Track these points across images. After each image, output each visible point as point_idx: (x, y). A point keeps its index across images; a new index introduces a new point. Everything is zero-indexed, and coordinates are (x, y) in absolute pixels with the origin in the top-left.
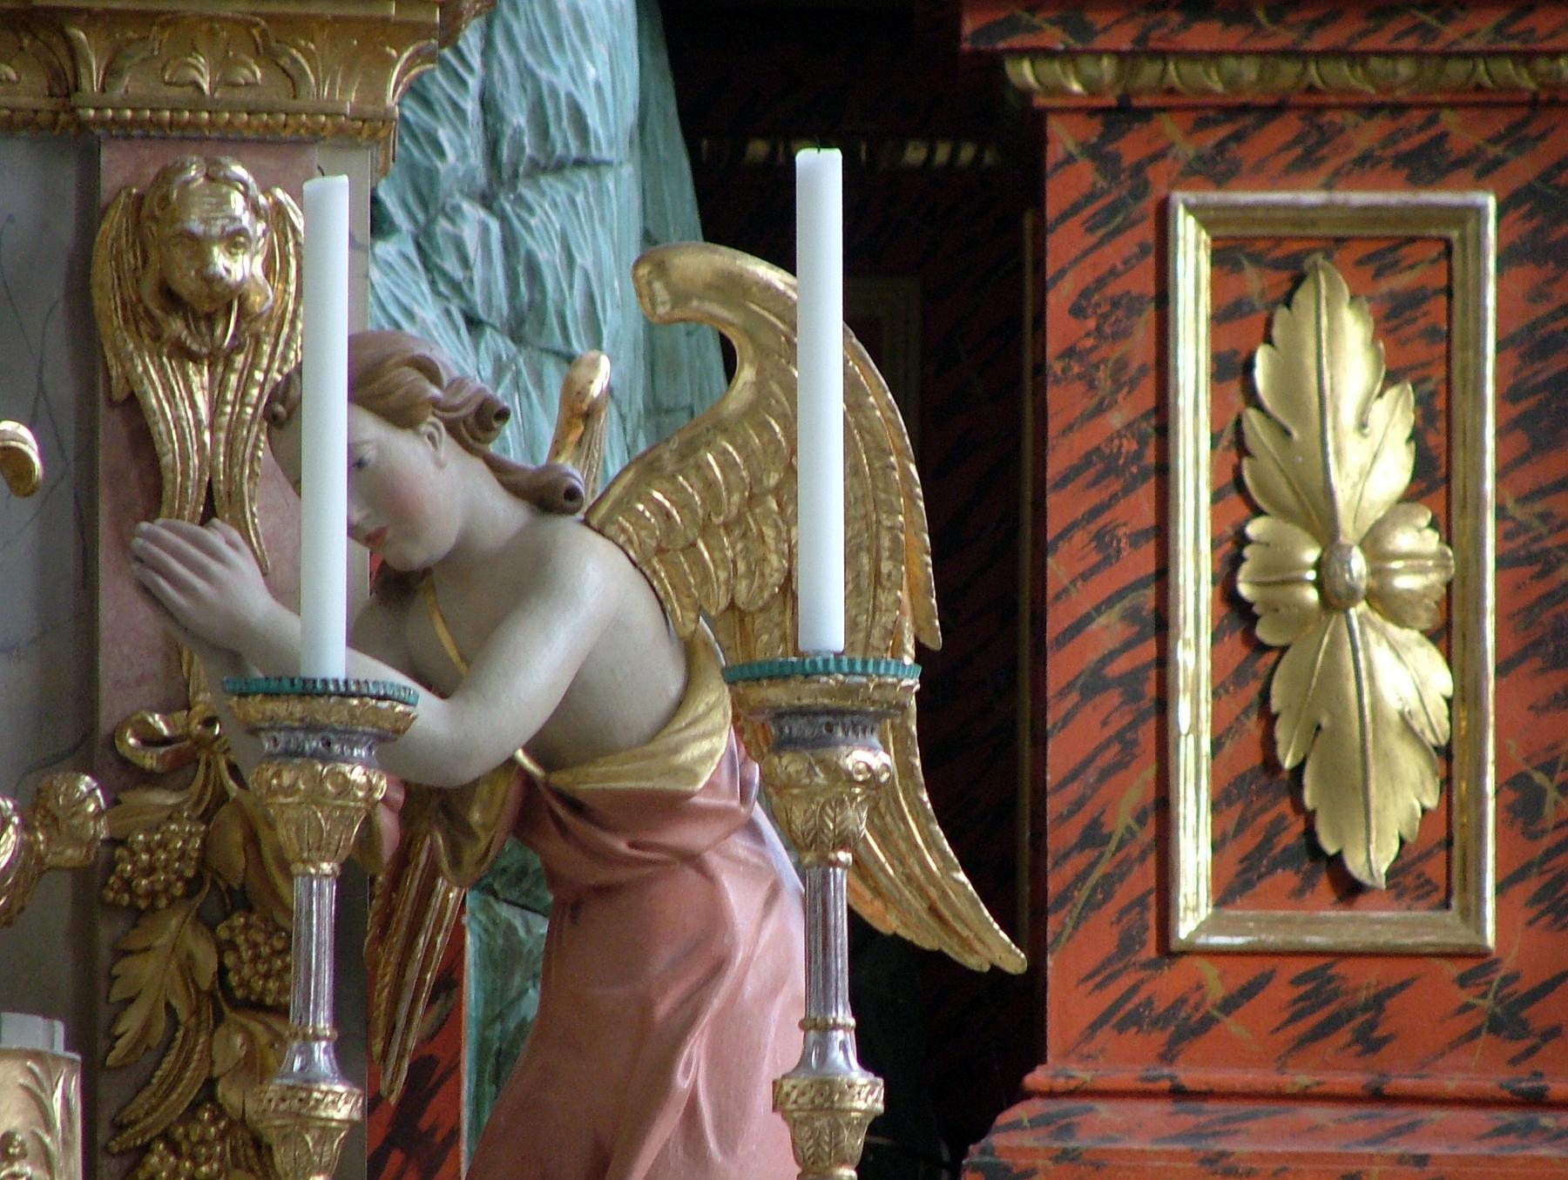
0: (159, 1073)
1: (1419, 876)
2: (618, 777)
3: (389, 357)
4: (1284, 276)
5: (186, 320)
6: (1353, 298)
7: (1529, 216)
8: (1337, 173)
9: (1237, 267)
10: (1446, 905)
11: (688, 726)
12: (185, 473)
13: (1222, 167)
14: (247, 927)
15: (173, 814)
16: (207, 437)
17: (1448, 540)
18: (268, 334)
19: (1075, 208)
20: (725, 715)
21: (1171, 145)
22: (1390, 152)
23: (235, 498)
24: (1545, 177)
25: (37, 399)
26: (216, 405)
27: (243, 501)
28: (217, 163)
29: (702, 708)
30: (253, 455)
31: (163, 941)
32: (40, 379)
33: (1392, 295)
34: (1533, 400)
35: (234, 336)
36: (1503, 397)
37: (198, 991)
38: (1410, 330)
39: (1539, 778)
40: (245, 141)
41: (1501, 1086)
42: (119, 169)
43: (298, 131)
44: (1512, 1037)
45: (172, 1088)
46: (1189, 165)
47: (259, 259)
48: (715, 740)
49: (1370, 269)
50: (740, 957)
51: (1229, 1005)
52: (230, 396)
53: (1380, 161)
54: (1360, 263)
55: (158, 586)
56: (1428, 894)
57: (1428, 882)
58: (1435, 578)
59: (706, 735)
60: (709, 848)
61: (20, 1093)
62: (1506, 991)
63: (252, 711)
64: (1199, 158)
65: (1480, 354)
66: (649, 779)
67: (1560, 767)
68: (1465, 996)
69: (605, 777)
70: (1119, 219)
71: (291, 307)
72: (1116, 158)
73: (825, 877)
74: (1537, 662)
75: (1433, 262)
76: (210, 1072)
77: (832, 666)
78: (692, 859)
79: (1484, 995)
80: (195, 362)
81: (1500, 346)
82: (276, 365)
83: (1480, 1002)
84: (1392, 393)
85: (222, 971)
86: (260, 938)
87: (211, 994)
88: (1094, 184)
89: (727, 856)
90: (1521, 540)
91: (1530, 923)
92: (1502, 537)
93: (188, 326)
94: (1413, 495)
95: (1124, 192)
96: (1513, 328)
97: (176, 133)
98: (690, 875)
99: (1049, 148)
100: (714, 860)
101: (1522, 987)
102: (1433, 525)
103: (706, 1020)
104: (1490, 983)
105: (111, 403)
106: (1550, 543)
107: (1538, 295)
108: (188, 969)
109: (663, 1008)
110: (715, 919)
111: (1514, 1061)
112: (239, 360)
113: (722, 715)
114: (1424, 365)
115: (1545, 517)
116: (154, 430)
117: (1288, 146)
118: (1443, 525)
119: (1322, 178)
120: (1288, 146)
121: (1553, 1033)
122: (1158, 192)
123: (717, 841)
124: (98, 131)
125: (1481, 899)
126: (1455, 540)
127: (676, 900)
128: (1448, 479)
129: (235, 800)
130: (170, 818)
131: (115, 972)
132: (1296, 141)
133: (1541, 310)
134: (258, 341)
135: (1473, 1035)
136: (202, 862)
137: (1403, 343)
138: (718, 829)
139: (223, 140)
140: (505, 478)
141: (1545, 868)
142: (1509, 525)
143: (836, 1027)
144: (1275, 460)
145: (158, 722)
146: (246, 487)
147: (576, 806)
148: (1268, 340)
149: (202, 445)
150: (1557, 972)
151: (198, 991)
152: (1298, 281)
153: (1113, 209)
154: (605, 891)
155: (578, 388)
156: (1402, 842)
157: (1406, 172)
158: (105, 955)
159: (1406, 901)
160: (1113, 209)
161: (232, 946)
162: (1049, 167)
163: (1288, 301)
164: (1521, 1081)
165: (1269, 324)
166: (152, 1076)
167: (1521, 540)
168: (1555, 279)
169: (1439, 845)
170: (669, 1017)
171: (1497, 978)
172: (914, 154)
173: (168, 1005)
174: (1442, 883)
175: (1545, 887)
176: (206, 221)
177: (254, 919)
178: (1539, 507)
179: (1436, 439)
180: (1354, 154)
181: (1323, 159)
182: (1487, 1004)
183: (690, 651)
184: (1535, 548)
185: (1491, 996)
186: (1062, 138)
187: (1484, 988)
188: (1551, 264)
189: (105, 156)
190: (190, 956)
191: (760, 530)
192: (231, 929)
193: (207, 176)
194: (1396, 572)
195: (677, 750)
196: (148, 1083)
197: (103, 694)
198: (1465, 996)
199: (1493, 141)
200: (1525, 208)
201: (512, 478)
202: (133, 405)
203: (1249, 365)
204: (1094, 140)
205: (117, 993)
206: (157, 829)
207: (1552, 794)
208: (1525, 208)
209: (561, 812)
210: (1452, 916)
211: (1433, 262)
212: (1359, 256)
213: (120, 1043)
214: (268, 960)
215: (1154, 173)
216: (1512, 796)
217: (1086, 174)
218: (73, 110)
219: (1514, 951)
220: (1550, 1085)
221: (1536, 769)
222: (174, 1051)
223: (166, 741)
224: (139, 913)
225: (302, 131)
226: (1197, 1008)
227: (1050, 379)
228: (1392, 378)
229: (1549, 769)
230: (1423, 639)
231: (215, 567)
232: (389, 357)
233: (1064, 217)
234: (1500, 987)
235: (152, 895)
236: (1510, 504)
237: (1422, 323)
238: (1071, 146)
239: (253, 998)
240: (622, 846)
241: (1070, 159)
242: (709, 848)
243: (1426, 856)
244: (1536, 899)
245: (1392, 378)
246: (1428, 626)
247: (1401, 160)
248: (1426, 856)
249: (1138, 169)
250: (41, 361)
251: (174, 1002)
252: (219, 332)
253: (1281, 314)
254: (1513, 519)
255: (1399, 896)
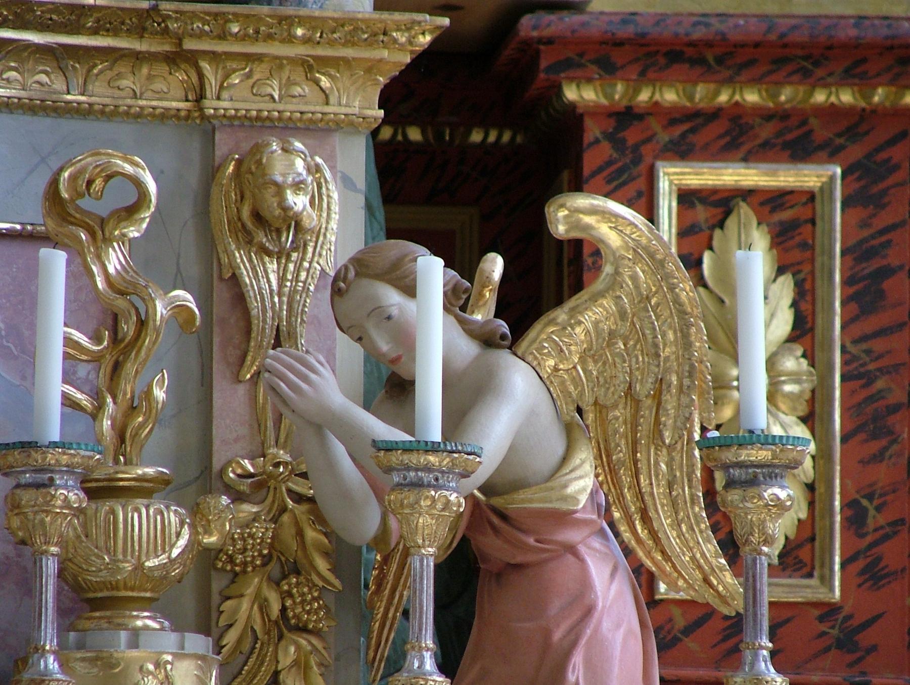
0: (246, 668)
1: (795, 558)
2: (531, 501)
3: (406, 255)
4: (719, 211)
5: (265, 231)
6: (759, 224)
7: (859, 179)
8: (750, 152)
9: (692, 205)
10: (810, 575)
11: (571, 471)
12: (264, 321)
13: (684, 148)
14: (298, 584)
15: (256, 518)
16: (276, 299)
17: (812, 364)
18: (310, 240)
19: (600, 170)
20: (591, 466)
21: (654, 135)
22: (780, 140)
23: (292, 336)
24: (869, 156)
25: (176, 275)
26: (282, 280)
27: (297, 338)
28: (289, 142)
29: (578, 462)
30: (302, 310)
31: (250, 591)
32: (178, 264)
33: (781, 223)
34: (861, 285)
35: (292, 242)
36: (845, 283)
37: (270, 620)
38: (791, 243)
39: (865, 502)
40: (297, 128)
41: (845, 680)
42: (223, 142)
43: (328, 123)
44: (850, 651)
45: (255, 677)
46: (665, 146)
47: (308, 197)
48: (587, 479)
49: (767, 208)
50: (600, 604)
51: (688, 631)
52: (289, 277)
53: (774, 145)
54: (762, 204)
55: (279, 385)
56: (801, 568)
57: (801, 561)
58: (807, 386)
59: (581, 477)
60: (580, 543)
61: (195, 678)
62: (845, 625)
63: (394, 459)
64: (671, 141)
65: (832, 257)
66: (551, 502)
67: (876, 496)
68: (823, 628)
69: (523, 501)
70: (626, 176)
71: (324, 226)
72: (623, 141)
73: (754, 560)
74: (861, 436)
75: (805, 204)
76: (277, 667)
77: (777, 441)
78: (572, 549)
79: (833, 627)
80: (269, 256)
81: (844, 253)
82: (316, 259)
83: (831, 631)
84: (781, 279)
85: (284, 609)
86: (306, 590)
87: (276, 622)
88: (611, 156)
89: (590, 548)
90: (855, 365)
91: (860, 586)
92: (845, 363)
93: (266, 236)
94: (792, 338)
95: (628, 161)
96: (851, 242)
97: (259, 124)
98: (570, 558)
99: (585, 135)
100: (582, 549)
101: (855, 622)
102: (804, 356)
103: (583, 641)
104: (836, 620)
105: (221, 278)
106: (871, 367)
107: (864, 224)
108: (264, 607)
109: (557, 635)
110: (585, 583)
111: (850, 665)
112: (294, 255)
113: (588, 468)
114: (798, 264)
115: (868, 352)
116: (246, 295)
117: (720, 137)
118: (808, 355)
119: (741, 155)
120: (720, 137)
121: (873, 649)
122: (648, 160)
123: (584, 539)
124: (215, 122)
125: (832, 570)
126: (817, 365)
127: (562, 573)
128: (812, 329)
129: (291, 510)
130: (254, 520)
131: (221, 609)
132: (727, 133)
133: (866, 233)
134: (305, 245)
135: (827, 650)
136: (271, 546)
137: (786, 250)
138: (585, 532)
139: (286, 128)
140: (466, 327)
141: (868, 554)
142: (848, 357)
143: (762, 648)
144: (713, 315)
145: (247, 464)
146: (298, 329)
147: (503, 516)
148: (711, 248)
149: (273, 303)
150: (875, 614)
151: (270, 620)
152: (727, 213)
153: (621, 171)
154: (519, 567)
155: (487, 275)
156: (787, 538)
157: (789, 152)
158: (216, 598)
159: (788, 572)
160: (621, 171)
161: (290, 594)
162: (585, 146)
163: (721, 225)
164: (855, 677)
165: (711, 238)
166: (242, 669)
167: (855, 365)
168: (874, 215)
169: (806, 540)
170: (561, 640)
171: (841, 617)
172: (476, 137)
173: (252, 628)
174: (809, 563)
175: (867, 566)
176: (284, 175)
177: (302, 579)
178: (864, 346)
179: (805, 306)
180: (758, 142)
181: (742, 144)
182: (835, 632)
183: (569, 429)
184: (862, 370)
185: (837, 626)
186: (593, 130)
187: (832, 623)
188: (872, 207)
189: (218, 136)
190: (266, 600)
191: (614, 360)
192: (290, 585)
193: (283, 149)
194: (784, 382)
195: (565, 486)
196: (240, 673)
197: (215, 448)
198: (823, 628)
199: (839, 135)
200: (856, 175)
201: (472, 327)
202: (235, 280)
203: (699, 262)
204: (611, 130)
205: (222, 622)
206: (247, 526)
207: (872, 512)
208: (856, 175)
209: (496, 520)
210: (814, 582)
211: (805, 204)
212: (762, 199)
213: (224, 650)
214: (310, 603)
215: (646, 150)
216: (849, 513)
217: (606, 150)
218: (201, 109)
219: (851, 602)
220: (873, 680)
221: (863, 497)
222: (255, 656)
223: (251, 476)
224: (236, 575)
225: (331, 124)
226: (669, 632)
227: (585, 268)
228: (781, 271)
229: (870, 497)
230: (799, 422)
231: (313, 376)
232: (406, 255)
233: (594, 174)
234: (842, 623)
235: (245, 564)
236: (848, 345)
237: (797, 239)
238: (598, 133)
239: (300, 625)
240: (531, 541)
241: (597, 141)
242: (580, 543)
243: (799, 546)
244: (862, 572)
245: (781, 271)
246: (801, 414)
247: (786, 146)
248: (799, 546)
249: (636, 147)
250: (179, 255)
251: (255, 627)
252: (283, 239)
253: (717, 233)
254: (850, 353)
255: (784, 570)
